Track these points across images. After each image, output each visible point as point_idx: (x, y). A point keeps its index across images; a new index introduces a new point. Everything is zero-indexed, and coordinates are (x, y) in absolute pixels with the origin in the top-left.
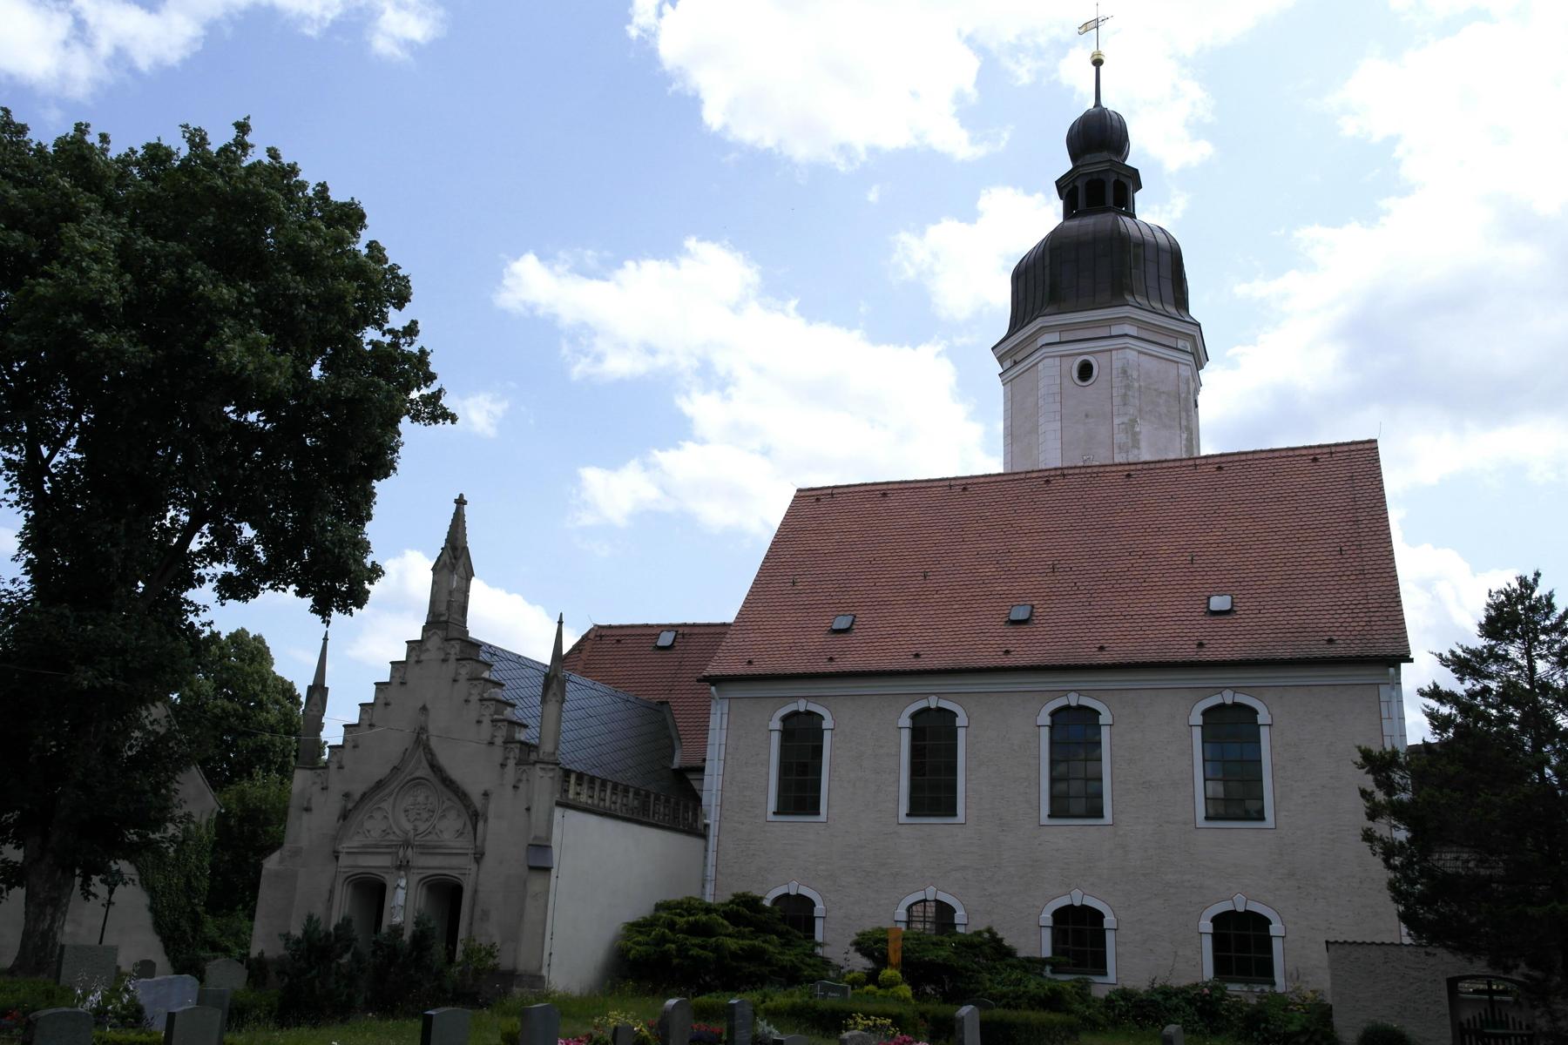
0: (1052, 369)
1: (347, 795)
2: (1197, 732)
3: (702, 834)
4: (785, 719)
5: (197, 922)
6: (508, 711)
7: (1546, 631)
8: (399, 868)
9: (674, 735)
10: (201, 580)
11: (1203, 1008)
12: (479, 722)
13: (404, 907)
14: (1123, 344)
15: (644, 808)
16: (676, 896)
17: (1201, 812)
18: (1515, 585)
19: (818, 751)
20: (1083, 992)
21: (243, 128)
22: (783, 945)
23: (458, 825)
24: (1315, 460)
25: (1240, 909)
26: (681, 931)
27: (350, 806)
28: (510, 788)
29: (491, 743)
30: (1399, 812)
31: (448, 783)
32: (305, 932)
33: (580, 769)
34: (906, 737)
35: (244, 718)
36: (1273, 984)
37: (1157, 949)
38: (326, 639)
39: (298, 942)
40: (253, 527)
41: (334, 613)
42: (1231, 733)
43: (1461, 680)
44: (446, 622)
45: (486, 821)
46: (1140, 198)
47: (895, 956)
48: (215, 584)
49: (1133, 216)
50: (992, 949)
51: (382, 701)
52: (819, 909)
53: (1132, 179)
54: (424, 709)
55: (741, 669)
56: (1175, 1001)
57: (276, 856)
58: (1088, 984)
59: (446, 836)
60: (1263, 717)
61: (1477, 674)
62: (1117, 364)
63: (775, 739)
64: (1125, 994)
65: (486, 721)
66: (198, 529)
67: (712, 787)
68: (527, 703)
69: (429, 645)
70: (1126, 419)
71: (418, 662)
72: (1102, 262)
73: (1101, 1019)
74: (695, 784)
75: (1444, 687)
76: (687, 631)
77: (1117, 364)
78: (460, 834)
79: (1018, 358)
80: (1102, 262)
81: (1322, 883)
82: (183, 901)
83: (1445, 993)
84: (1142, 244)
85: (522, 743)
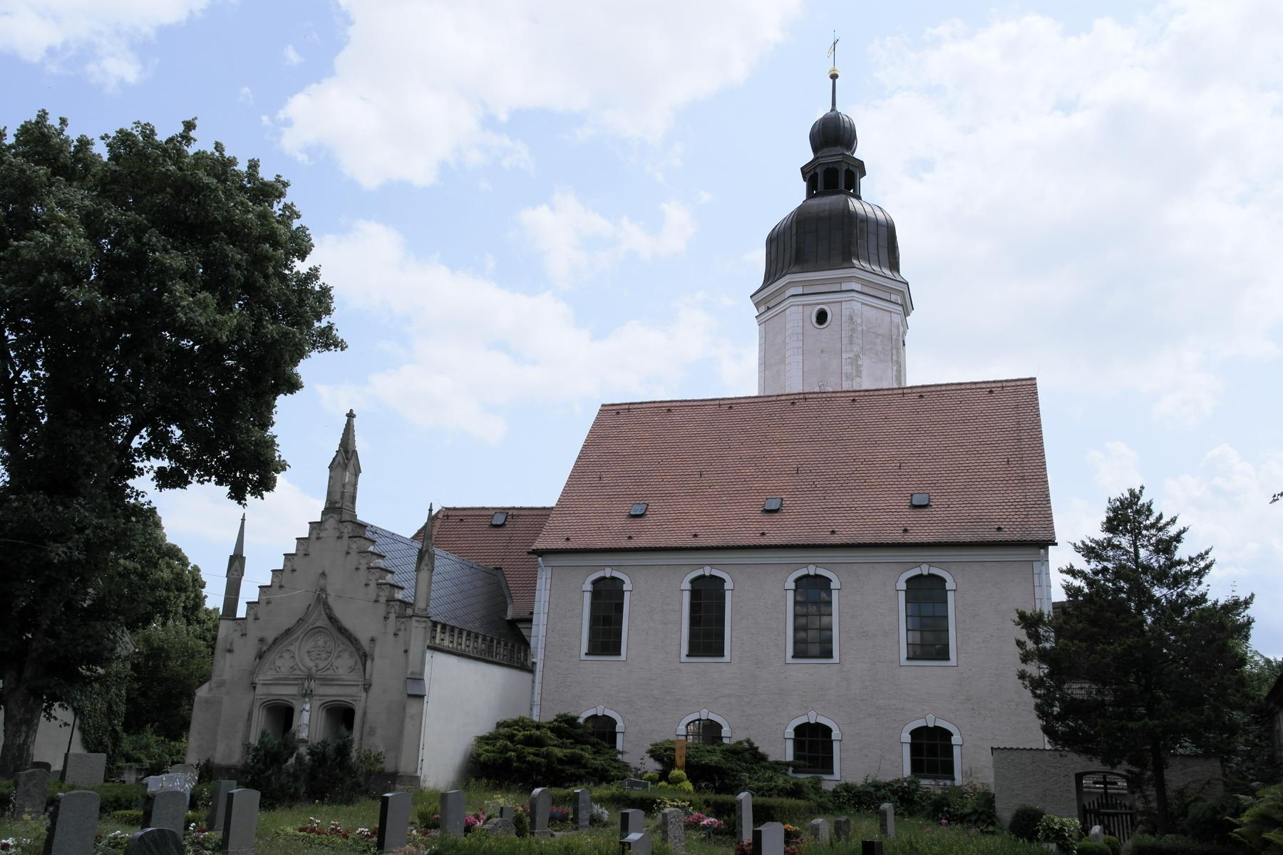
0: (797, 315)
1: (262, 640)
2: (902, 596)
3: (531, 670)
4: (595, 583)
5: (116, 739)
6: (389, 578)
7: (1147, 528)
8: (305, 695)
9: (506, 592)
10: (141, 472)
11: (905, 797)
12: (367, 585)
13: (309, 726)
14: (849, 292)
15: (489, 650)
16: (514, 716)
18: (1127, 495)
19: (619, 608)
20: (816, 788)
21: (189, 126)
22: (595, 753)
23: (351, 662)
24: (991, 392)
25: (931, 725)
26: (519, 743)
28: (391, 636)
29: (376, 601)
30: (1043, 656)
31: (342, 630)
32: (261, 742)
34: (686, 597)
35: (143, 576)
36: (953, 779)
37: (870, 753)
38: (243, 520)
39: (256, 749)
40: (180, 427)
41: (248, 496)
42: (926, 594)
43: (1088, 562)
44: (341, 508)
46: (864, 183)
47: (680, 761)
48: (152, 474)
49: (859, 198)
50: (749, 755)
52: (620, 726)
53: (858, 169)
54: (323, 574)
55: (561, 545)
56: (883, 792)
57: (206, 686)
58: (820, 780)
59: (340, 671)
60: (950, 585)
61: (1099, 558)
62: (846, 313)
63: (587, 598)
64: (847, 788)
65: (373, 584)
66: (138, 432)
67: (538, 634)
68: (403, 568)
69: (327, 525)
70: (851, 355)
71: (318, 538)
72: (831, 232)
73: (830, 805)
74: (525, 632)
75: (1077, 567)
76: (515, 512)
77: (846, 313)
78: (352, 670)
79: (770, 305)
80: (831, 232)
81: (989, 707)
82: (105, 723)
83: (1074, 784)
84: (865, 220)
85: (400, 601)
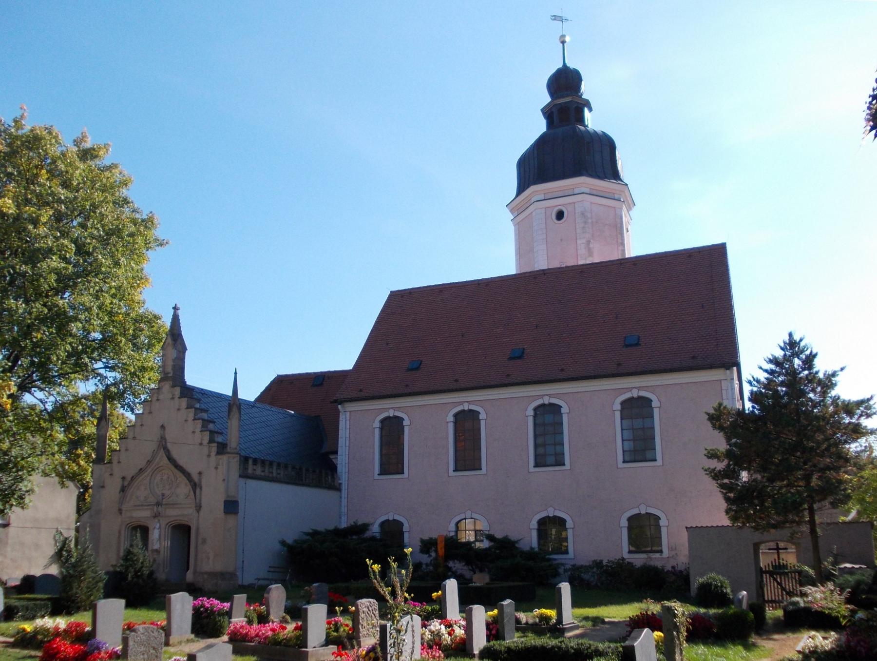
1: (123, 478)
2: (618, 415)
3: (338, 489)
8: (155, 517)
17: (620, 458)
27: (126, 484)
29: (201, 444)
33: (254, 456)
38: (236, 373)
45: (201, 488)
51: (139, 424)
52: (406, 527)
54: (163, 427)
67: (342, 460)
71: (158, 400)
78: (187, 497)
